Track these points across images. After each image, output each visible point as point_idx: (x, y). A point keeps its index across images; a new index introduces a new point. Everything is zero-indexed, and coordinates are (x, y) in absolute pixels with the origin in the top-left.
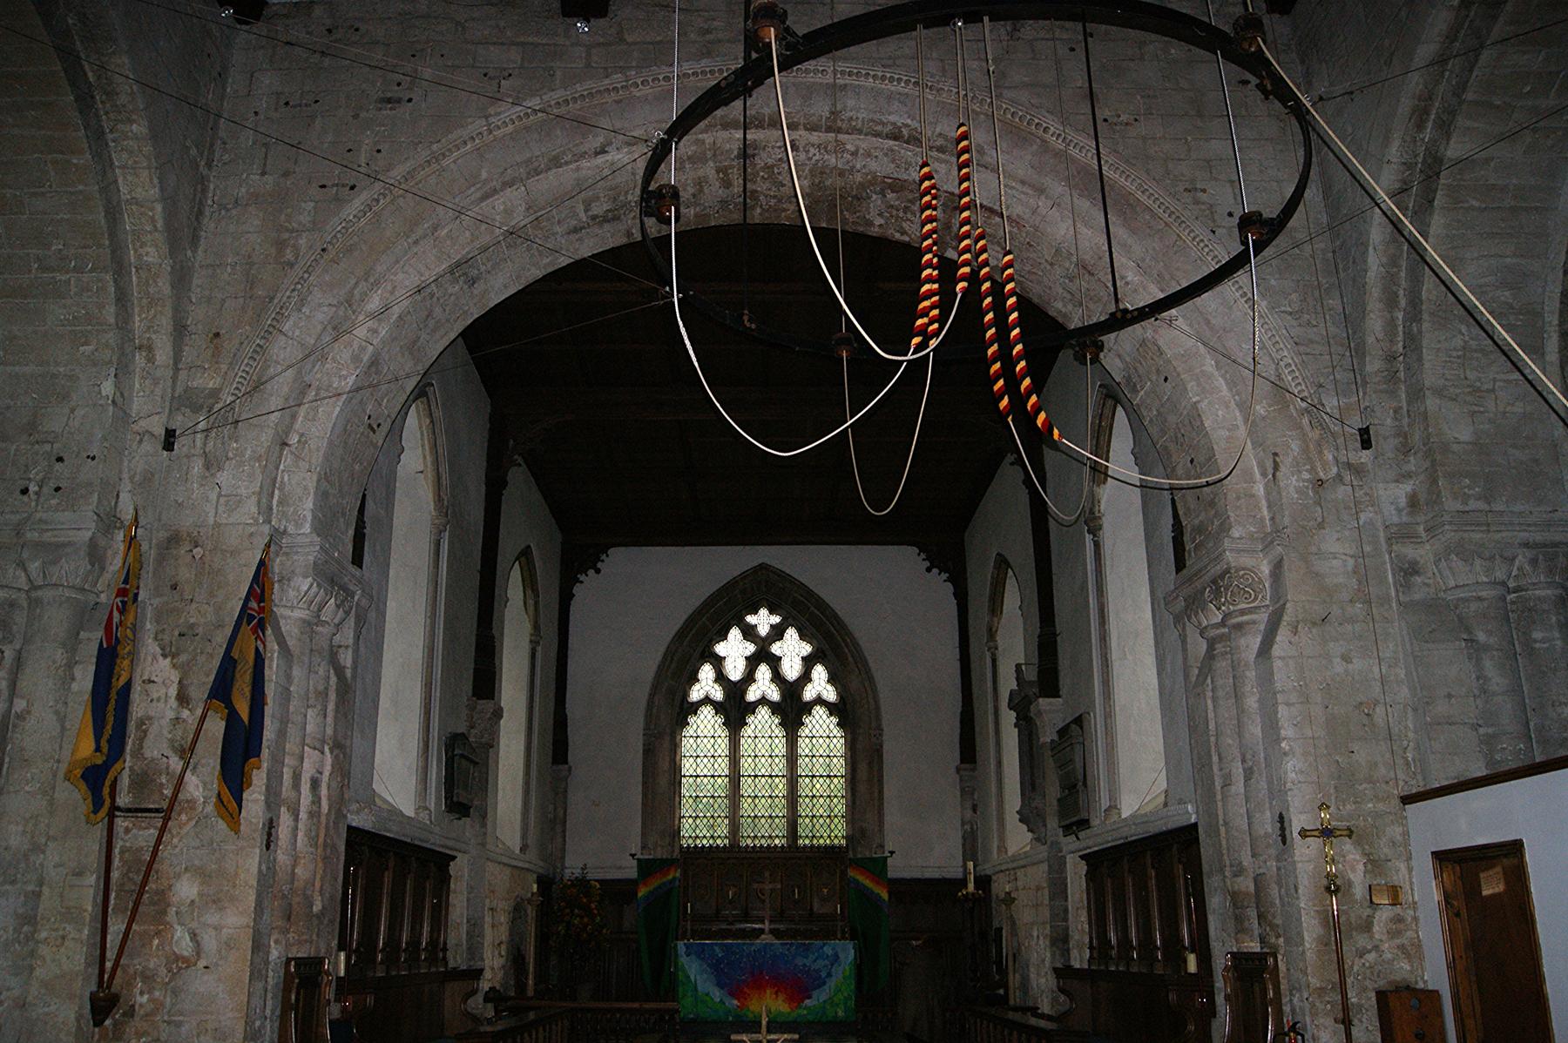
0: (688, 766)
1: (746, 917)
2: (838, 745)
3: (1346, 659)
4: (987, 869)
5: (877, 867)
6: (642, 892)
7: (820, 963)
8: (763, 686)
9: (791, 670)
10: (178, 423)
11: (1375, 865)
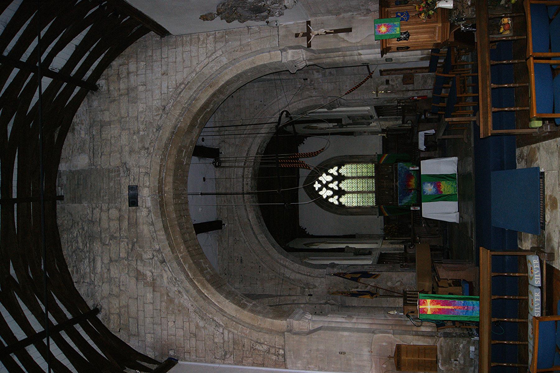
0: (355, 204)
1: (393, 189)
2: (348, 166)
4: (380, 130)
7: (403, 171)
8: (334, 185)
9: (330, 178)
11: (382, 84)
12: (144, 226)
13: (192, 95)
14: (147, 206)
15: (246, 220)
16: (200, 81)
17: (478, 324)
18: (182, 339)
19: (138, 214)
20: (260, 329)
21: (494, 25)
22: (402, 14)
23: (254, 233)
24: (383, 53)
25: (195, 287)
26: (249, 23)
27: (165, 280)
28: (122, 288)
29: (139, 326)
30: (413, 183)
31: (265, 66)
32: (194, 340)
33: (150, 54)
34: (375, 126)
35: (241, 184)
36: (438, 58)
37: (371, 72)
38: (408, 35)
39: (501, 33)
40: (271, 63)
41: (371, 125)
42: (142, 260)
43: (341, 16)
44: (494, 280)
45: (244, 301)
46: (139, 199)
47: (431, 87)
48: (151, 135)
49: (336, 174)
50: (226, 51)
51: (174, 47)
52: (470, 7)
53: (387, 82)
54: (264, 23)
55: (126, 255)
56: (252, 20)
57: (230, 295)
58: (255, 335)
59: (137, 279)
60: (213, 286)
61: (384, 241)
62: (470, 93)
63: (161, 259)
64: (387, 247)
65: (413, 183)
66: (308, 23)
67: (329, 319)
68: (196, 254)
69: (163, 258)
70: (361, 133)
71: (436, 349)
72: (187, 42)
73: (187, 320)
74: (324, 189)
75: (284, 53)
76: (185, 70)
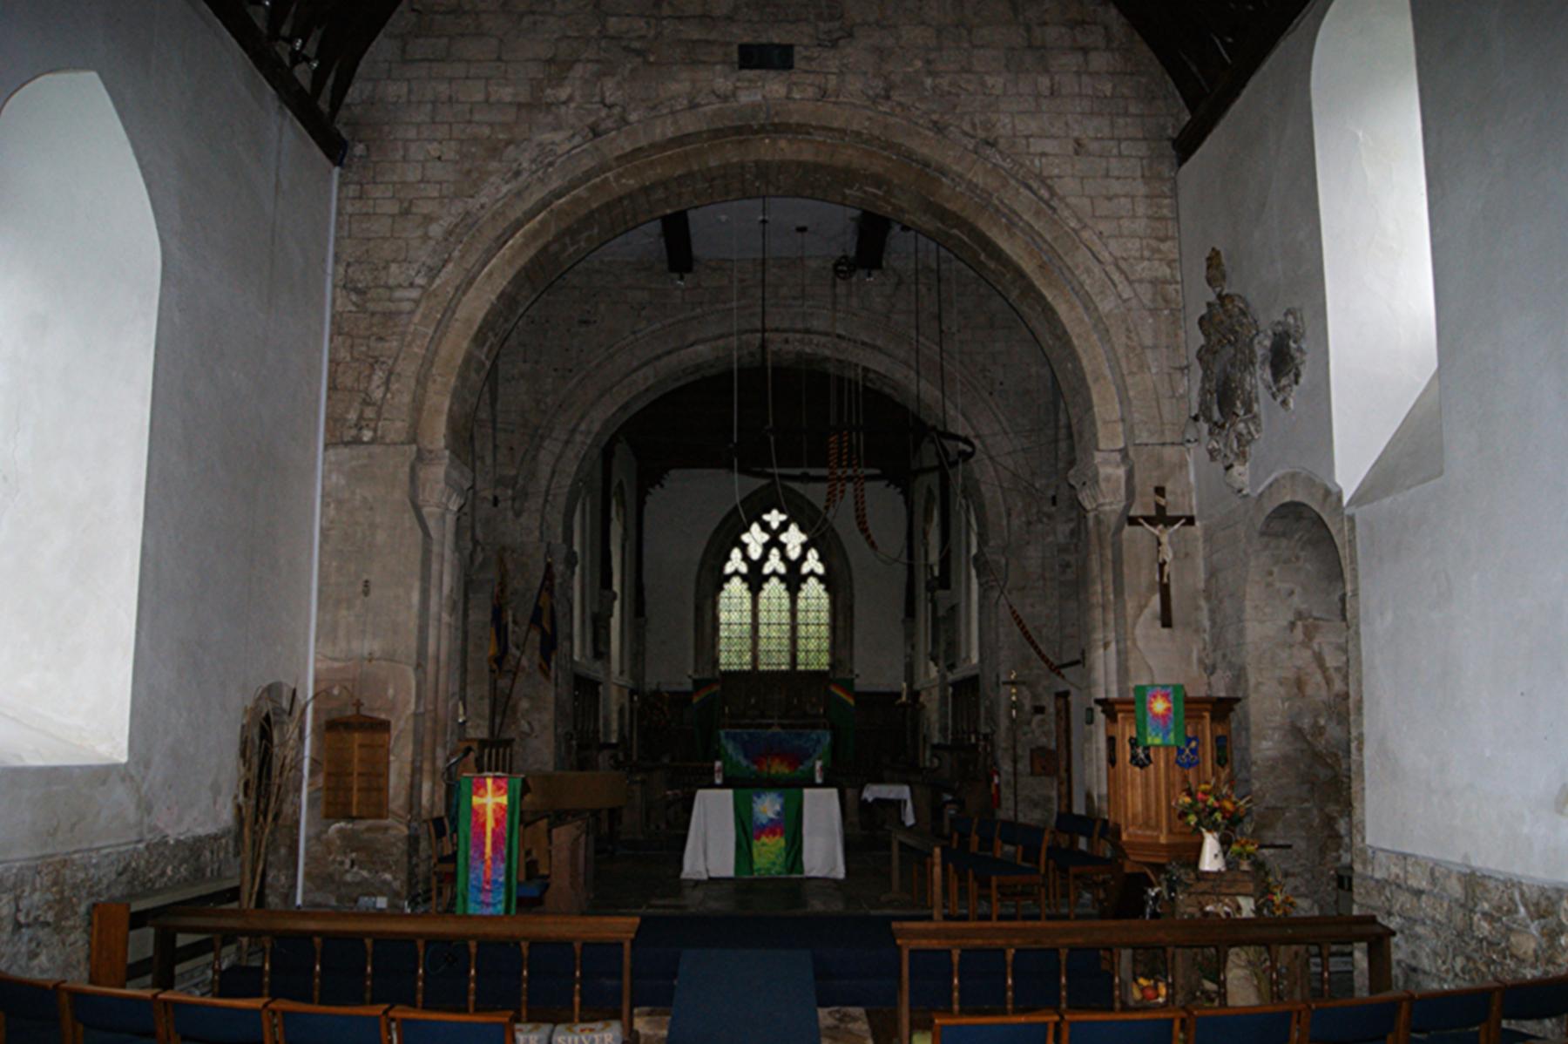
0: (723, 617)
2: (825, 601)
3: (1032, 606)
4: (917, 687)
5: (848, 685)
6: (696, 700)
8: (774, 563)
10: (498, 492)
11: (1035, 696)
12: (687, 84)
13: (1021, 219)
14: (739, 93)
15: (692, 338)
16: (1055, 239)
17: (450, 909)
18: (395, 178)
19: (718, 67)
20: (422, 381)
21: (1153, 962)
22: (1194, 751)
23: (658, 357)
24: (1105, 703)
25: (530, 215)
26: (1197, 372)
27: (547, 137)
28: (527, 21)
29: (427, 64)
30: (779, 769)
31: (1089, 407)
32: (393, 208)
33: (1132, 109)
34: (927, 673)
35: (786, 324)
36: (1089, 836)
37: (1063, 671)
38: (1142, 764)
39: (1135, 980)
40: (1093, 423)
41: (931, 664)
42: (599, 76)
43: (1202, 603)
44: (564, 945)
45: (492, 339)
46: (758, 72)
47: (1021, 819)
48: (923, 107)
49: (805, 569)
50: (1129, 310)
51: (1147, 174)
52: (1202, 909)
53: (1039, 710)
54: (1194, 412)
55: (612, 32)
56: (1203, 381)
57: (507, 301)
58: (409, 369)
59: (550, 61)
60: (531, 261)
61: (626, 692)
62: (997, 909)
63: (603, 127)
64: (613, 699)
65: (779, 769)
66: (1190, 521)
67: (448, 553)
68: (613, 217)
69: (607, 131)
70: (910, 637)
71: (380, 816)
72: (1160, 207)
73: (445, 192)
74: (766, 537)
75: (1118, 457)
76: (1086, 201)
